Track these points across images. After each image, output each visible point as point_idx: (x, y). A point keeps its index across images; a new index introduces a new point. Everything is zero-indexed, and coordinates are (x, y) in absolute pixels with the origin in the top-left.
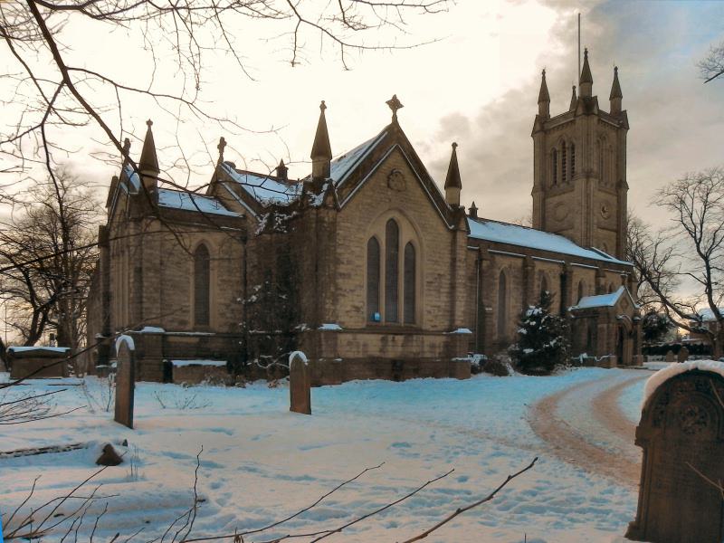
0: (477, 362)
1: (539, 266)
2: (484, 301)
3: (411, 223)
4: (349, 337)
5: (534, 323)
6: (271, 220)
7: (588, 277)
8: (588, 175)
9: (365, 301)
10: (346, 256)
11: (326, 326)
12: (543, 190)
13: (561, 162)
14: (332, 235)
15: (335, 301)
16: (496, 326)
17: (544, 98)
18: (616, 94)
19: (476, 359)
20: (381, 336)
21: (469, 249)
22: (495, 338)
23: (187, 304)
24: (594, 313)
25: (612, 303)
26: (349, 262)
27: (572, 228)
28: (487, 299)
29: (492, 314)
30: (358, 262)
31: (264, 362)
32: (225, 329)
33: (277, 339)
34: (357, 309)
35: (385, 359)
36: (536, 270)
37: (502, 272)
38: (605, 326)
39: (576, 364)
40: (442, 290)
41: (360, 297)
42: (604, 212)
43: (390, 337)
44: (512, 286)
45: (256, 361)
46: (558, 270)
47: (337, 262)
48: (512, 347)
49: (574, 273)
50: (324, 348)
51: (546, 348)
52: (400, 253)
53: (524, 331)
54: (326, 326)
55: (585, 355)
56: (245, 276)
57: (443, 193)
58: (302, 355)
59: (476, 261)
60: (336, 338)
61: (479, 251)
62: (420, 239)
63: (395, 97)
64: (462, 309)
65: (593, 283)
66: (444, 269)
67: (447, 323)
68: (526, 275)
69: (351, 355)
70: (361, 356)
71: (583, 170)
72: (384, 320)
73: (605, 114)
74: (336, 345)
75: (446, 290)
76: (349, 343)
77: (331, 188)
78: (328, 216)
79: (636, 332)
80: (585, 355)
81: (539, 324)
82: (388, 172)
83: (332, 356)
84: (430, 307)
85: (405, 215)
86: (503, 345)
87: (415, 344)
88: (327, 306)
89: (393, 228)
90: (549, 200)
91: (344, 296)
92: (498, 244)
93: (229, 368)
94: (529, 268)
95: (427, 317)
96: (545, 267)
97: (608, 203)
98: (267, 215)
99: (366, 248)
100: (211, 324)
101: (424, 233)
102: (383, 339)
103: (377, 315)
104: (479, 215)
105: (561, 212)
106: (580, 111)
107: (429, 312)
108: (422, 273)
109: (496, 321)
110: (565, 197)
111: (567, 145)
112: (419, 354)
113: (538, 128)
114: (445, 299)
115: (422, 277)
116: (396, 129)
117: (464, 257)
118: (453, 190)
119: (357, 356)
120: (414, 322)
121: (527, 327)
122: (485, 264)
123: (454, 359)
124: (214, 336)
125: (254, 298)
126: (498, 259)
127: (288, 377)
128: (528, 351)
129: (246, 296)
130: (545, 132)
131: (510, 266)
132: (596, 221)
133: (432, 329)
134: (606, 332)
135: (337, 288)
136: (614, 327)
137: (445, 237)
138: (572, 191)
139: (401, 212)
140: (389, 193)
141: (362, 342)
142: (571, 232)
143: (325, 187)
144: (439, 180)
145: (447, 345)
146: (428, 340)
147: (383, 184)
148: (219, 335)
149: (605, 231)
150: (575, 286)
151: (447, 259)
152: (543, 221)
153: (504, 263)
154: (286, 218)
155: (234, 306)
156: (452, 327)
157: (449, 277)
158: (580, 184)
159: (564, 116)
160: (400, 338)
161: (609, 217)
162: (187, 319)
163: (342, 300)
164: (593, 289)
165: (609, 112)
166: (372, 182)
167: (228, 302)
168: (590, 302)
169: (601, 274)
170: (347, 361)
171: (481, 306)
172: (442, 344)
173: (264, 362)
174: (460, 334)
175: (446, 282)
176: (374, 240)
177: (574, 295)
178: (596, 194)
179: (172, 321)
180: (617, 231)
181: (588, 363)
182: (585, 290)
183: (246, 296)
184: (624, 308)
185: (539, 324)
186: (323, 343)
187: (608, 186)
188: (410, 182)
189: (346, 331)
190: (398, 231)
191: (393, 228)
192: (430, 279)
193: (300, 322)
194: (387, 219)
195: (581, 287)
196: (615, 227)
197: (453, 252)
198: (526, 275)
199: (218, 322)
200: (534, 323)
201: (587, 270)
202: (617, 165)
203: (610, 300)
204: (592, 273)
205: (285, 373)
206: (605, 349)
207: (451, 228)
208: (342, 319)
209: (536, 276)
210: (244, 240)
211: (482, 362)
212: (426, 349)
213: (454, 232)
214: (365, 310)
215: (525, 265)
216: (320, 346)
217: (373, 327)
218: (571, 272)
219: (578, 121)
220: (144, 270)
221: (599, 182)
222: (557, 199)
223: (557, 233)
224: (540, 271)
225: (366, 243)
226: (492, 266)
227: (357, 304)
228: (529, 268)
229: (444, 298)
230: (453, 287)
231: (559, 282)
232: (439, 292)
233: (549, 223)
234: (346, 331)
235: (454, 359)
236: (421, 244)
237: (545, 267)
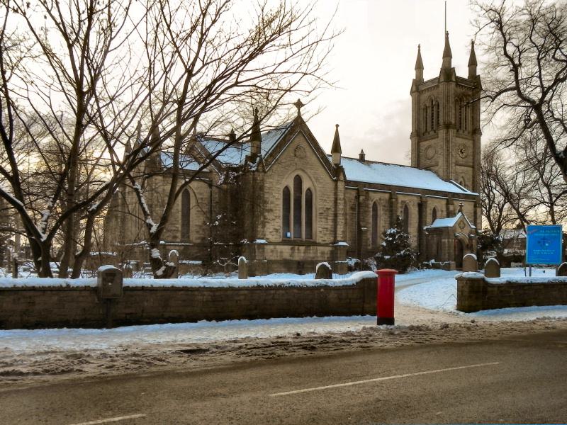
0: (353, 264)
1: (401, 198)
2: (362, 223)
3: (310, 178)
4: (272, 247)
5: (391, 239)
6: (227, 177)
7: (441, 204)
8: (448, 126)
9: (281, 225)
10: (271, 199)
11: (259, 241)
12: (419, 136)
13: (430, 115)
14: (262, 188)
15: (264, 226)
16: (371, 239)
17: (419, 66)
18: (473, 63)
19: (352, 262)
20: (290, 247)
22: (370, 248)
24: (440, 231)
25: (451, 225)
26: (272, 203)
27: (437, 165)
28: (363, 221)
29: (366, 232)
30: (277, 203)
31: (223, 262)
32: (199, 241)
33: (230, 248)
34: (277, 230)
35: (292, 261)
36: (400, 201)
37: (375, 203)
38: (446, 240)
39: (428, 267)
40: (329, 218)
41: (279, 223)
42: (462, 153)
43: (297, 247)
44: (382, 212)
45: (218, 261)
46: (416, 200)
47: (265, 202)
48: (378, 255)
49: (429, 203)
50: (257, 254)
51: (398, 256)
53: (384, 244)
54: (259, 241)
55: (433, 261)
56: (211, 208)
58: (244, 258)
60: (264, 248)
61: (358, 190)
63: (299, 100)
64: (342, 230)
65: (444, 209)
66: (330, 205)
67: (332, 238)
68: (391, 205)
69: (273, 258)
70: (279, 258)
71: (444, 123)
72: (292, 236)
73: (462, 80)
74: (264, 251)
76: (272, 251)
77: (261, 159)
78: (259, 177)
79: (472, 245)
80: (433, 261)
81: (394, 239)
82: (295, 147)
83: (262, 258)
84: (321, 229)
85: (306, 173)
86: (371, 254)
87: (311, 251)
88: (259, 229)
89: (298, 181)
90: (422, 144)
91: (268, 222)
92: (370, 185)
93: (203, 265)
94: (394, 200)
96: (406, 199)
97: (465, 146)
98: (225, 173)
99: (282, 193)
100: (191, 239)
101: (318, 183)
102: (292, 249)
103: (289, 234)
104: (367, 158)
105: (430, 153)
106: (442, 80)
107: (321, 232)
108: (316, 209)
109: (370, 236)
110: (432, 142)
112: (314, 258)
113: (414, 89)
114: (331, 224)
115: (316, 209)
116: (299, 121)
117: (343, 197)
119: (276, 258)
121: (387, 241)
122: (361, 198)
123: (336, 262)
124: (192, 246)
125: (217, 223)
126: (371, 194)
127: (237, 271)
128: (387, 257)
129: (212, 221)
130: (419, 92)
131: (380, 199)
132: (454, 161)
133: (322, 243)
134: (447, 245)
135: (265, 218)
136: (452, 241)
137: (331, 185)
138: (438, 137)
139: (303, 171)
140: (296, 160)
141: (279, 250)
142: (436, 168)
143: (258, 159)
144: (327, 148)
145: (332, 252)
148: (196, 245)
149: (463, 168)
150: (429, 211)
151: (332, 198)
152: (420, 162)
153: (375, 197)
154: (236, 174)
155: (204, 227)
156: (335, 241)
157: (333, 210)
158: (442, 133)
159: (432, 81)
160: (302, 248)
161: (466, 157)
162: (177, 235)
163: (268, 225)
164: (445, 213)
165: (467, 78)
166: (286, 153)
167: (200, 224)
168: (441, 223)
169: (450, 202)
170: (270, 262)
171: (359, 227)
173: (223, 262)
174: (340, 246)
175: (331, 212)
177: (429, 218)
178: (453, 140)
179: (168, 237)
180: (473, 167)
181: (435, 267)
182: (439, 214)
183: (212, 221)
184: (462, 228)
185: (394, 239)
186: (257, 251)
187: (466, 132)
188: (309, 152)
189: (270, 243)
191: (298, 181)
193: (244, 238)
194: (295, 175)
195: (434, 211)
196: (471, 164)
197: (336, 194)
198: (391, 205)
199: (194, 237)
200: (391, 239)
201: (438, 200)
202: (473, 117)
203: (450, 222)
204: (444, 202)
205: (235, 268)
206: (447, 256)
207: (335, 178)
208: (267, 237)
209: (400, 205)
210: (211, 186)
211: (356, 264)
212: (319, 255)
213: (336, 181)
214: (281, 231)
215: (391, 198)
216: (255, 253)
217: (286, 241)
218: (426, 202)
220: (153, 206)
221: (458, 131)
223: (427, 169)
224: (402, 201)
225: (282, 191)
226: (367, 198)
227: (277, 228)
228: (394, 200)
229: (330, 223)
230: (336, 215)
231: (417, 209)
232: (327, 219)
233: (423, 161)
234: (270, 243)
235: (336, 262)
237: (406, 199)
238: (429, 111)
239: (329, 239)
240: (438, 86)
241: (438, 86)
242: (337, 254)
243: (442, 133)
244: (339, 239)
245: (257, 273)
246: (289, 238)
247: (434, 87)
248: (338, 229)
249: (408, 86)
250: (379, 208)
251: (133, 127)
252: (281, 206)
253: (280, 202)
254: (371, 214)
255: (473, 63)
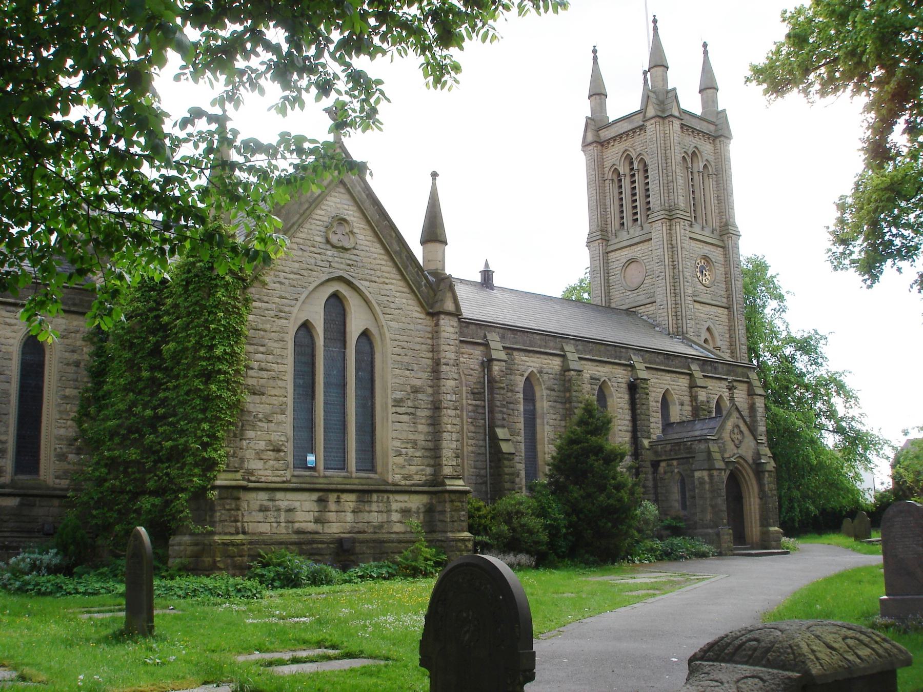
8: (670, 217)
16: (523, 473)
17: (598, 93)
18: (708, 87)
21: (461, 341)
23: (394, 380)
40: (419, 413)
44: (546, 404)
52: (348, 351)
57: (418, 251)
59: (483, 363)
62: (380, 327)
65: (687, 399)
66: (420, 378)
72: (321, 467)
75: (427, 413)
76: (263, 509)
90: (612, 256)
95: (393, 460)
96: (602, 371)
103: (311, 458)
104: (497, 281)
109: (521, 467)
111: (635, 166)
112: (381, 526)
117: (453, 356)
118: (431, 246)
120: (373, 469)
132: (690, 291)
139: (349, 284)
144: (411, 235)
145: (429, 510)
146: (399, 502)
147: (319, 239)
158: (658, 231)
160: (349, 500)
172: (422, 510)
176: (306, 327)
190: (344, 310)
192: (399, 395)
197: (434, 349)
214: (289, 448)
219: (650, 126)
222: (625, 254)
231: (627, 397)
236: (382, 335)
238: (626, 183)
239: (419, 472)
240: (642, 128)
241: (642, 128)
242: (443, 512)
243: (658, 231)
244: (447, 471)
245: (440, 258)
246: (313, 469)
247: (633, 130)
248: (444, 444)
249: (577, 132)
250: (538, 394)
251: (378, 506)
252: (289, 377)
253: (288, 367)
254: (521, 408)
255: (708, 87)
